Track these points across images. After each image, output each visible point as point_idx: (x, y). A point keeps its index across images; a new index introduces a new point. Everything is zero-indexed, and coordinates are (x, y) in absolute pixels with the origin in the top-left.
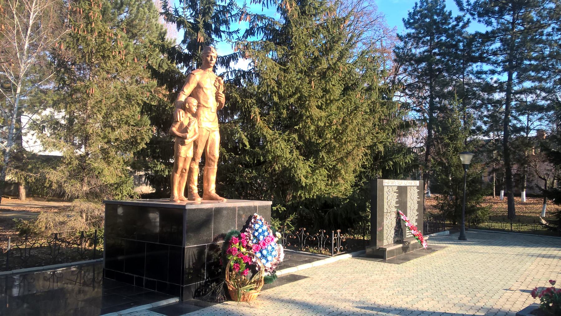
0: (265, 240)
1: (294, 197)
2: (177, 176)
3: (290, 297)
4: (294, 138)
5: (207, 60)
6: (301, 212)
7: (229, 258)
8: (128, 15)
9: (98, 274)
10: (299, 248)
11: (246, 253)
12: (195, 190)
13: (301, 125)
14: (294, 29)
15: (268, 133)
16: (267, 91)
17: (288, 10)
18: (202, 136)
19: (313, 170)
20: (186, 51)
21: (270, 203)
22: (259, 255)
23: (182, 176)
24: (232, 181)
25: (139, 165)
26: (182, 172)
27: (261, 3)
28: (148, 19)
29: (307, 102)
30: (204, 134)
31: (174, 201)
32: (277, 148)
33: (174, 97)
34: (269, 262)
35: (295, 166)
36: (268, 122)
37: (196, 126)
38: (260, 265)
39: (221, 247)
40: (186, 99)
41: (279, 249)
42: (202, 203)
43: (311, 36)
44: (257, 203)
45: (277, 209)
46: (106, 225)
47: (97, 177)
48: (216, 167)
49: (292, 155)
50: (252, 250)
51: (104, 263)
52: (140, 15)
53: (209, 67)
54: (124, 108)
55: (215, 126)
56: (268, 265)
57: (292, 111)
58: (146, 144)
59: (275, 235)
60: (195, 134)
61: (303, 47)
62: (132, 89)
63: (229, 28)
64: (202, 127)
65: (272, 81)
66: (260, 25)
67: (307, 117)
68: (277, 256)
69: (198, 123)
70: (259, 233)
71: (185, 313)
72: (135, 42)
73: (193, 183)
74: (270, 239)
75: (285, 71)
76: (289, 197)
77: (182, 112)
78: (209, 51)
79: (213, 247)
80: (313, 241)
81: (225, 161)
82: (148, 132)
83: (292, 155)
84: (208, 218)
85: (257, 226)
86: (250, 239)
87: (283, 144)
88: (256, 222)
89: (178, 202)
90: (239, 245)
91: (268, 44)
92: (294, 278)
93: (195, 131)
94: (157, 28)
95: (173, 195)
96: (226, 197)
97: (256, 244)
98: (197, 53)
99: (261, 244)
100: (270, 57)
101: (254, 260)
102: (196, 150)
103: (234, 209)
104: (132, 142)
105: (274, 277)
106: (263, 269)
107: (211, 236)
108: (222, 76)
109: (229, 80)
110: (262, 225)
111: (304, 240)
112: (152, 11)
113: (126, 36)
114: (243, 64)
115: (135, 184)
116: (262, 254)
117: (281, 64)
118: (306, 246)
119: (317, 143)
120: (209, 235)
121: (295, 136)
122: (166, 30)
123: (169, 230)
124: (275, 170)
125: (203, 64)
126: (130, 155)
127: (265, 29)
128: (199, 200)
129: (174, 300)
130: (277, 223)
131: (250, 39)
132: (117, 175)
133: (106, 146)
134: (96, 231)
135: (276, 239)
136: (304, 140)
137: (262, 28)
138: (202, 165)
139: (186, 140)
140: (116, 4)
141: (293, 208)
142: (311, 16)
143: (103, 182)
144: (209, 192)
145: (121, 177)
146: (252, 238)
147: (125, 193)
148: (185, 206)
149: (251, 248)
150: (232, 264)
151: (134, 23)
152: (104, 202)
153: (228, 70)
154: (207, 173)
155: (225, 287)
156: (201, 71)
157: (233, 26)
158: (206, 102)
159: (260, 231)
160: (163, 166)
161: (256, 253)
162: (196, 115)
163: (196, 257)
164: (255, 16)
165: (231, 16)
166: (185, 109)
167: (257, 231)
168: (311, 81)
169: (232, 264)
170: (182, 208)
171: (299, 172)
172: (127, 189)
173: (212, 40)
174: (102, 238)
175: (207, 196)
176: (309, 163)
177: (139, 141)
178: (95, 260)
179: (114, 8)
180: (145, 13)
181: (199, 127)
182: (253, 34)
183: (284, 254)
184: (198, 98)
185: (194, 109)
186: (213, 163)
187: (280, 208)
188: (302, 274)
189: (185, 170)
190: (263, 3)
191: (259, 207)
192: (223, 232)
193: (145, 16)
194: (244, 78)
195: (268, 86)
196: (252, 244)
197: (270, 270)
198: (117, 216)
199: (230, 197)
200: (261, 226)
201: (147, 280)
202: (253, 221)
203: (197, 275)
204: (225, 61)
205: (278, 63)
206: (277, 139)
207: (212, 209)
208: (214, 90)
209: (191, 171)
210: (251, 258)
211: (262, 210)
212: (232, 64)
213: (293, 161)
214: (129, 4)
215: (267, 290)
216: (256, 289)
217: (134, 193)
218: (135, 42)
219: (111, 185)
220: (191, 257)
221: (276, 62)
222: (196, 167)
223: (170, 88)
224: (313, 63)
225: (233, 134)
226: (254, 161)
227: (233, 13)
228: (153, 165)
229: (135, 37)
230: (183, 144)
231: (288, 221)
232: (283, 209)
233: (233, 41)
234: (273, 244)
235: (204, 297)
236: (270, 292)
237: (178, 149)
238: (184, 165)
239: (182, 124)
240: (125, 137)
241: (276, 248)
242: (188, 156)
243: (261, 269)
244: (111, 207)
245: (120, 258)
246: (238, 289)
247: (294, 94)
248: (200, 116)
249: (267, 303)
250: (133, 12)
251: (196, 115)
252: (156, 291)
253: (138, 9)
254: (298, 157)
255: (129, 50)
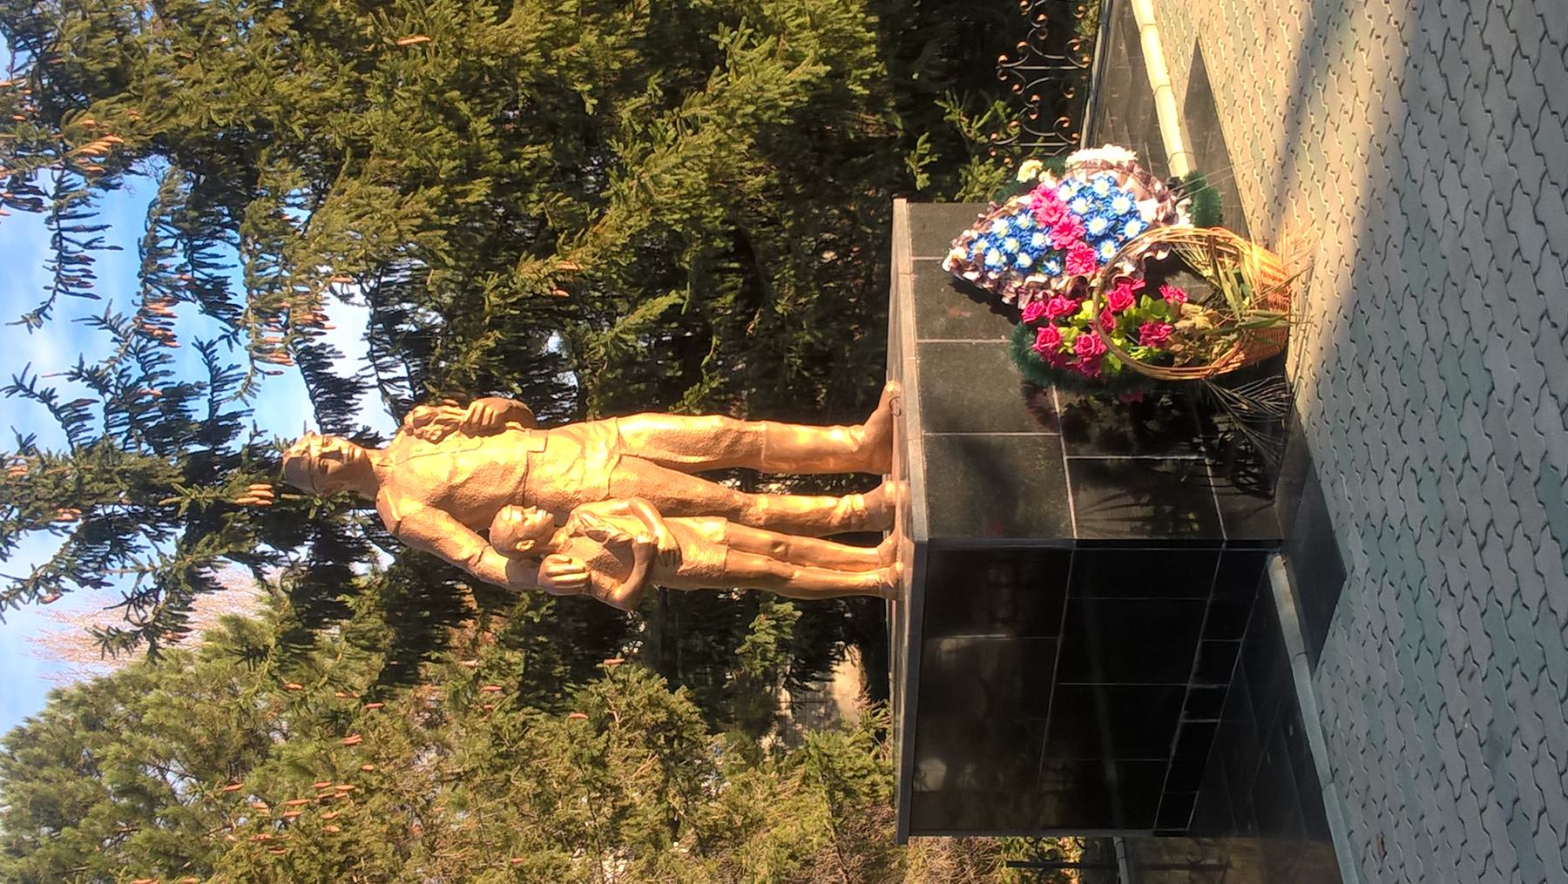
0: (1049, 225)
1: (874, 104)
2: (803, 575)
3: (1277, 120)
4: (634, 112)
5: (338, 473)
6: (934, 73)
7: (1118, 366)
8: (174, 765)
9: (1173, 851)
10: (1080, 80)
11: (1100, 300)
12: (855, 502)
13: (579, 87)
14: (186, 120)
15: (617, 224)
16: (449, 227)
17: (113, 145)
18: (641, 484)
19: (766, 27)
20: (303, 553)
21: (901, 206)
22: (1108, 250)
23: (799, 558)
24: (817, 358)
25: (752, 706)
26: (783, 558)
27: (88, 253)
28: (185, 688)
29: (487, 60)
30: (634, 477)
31: (899, 582)
32: (680, 183)
33: (492, 594)
34: (1139, 206)
35: (750, 109)
36: (577, 225)
37: (602, 508)
38: (1148, 241)
39: (1075, 400)
40: (501, 551)
41: (1086, 165)
42: (905, 476)
43: (210, 47)
44: (903, 259)
45: (925, 169)
46: (990, 828)
47: (808, 863)
48: (762, 427)
49: (706, 120)
50: (1089, 275)
51: (1131, 834)
52: (171, 723)
53: (365, 462)
54: (541, 776)
55: (602, 434)
56: (1149, 209)
57: (524, 118)
58: (672, 688)
59: (1031, 186)
60: (633, 511)
61: (255, 81)
62: (468, 744)
63: (200, 386)
64: (605, 483)
65: (406, 209)
66: (180, 259)
67: (549, 61)
68: (1114, 174)
69: (589, 501)
70: (1023, 247)
71: (1331, 532)
72: (277, 736)
73: (828, 513)
74: (1046, 204)
75: (362, 151)
76: (872, 125)
77: (550, 565)
78: (304, 466)
79: (1074, 426)
80: (1049, 23)
81: (734, 386)
82: (629, 683)
83: (706, 120)
84: (961, 445)
85: (994, 258)
86: (1047, 285)
87: (663, 160)
88: (979, 263)
89: (903, 567)
90: (1068, 325)
91: (255, 225)
92: (1201, 104)
93: (622, 513)
94: (218, 656)
95: (875, 588)
96: (882, 383)
97: (1063, 263)
98: (312, 512)
99: (1065, 240)
100: (304, 215)
101: (1128, 268)
102: (699, 505)
103: (925, 352)
104: (674, 748)
105: (1193, 185)
106: (1164, 233)
107: (1033, 441)
108: (399, 409)
109: (410, 378)
110: (993, 239)
111: (1046, 62)
112: (153, 677)
113: (258, 771)
114: (347, 328)
115: (828, 716)
116: (1105, 237)
117: (333, 172)
118: (1072, 53)
119: (652, 15)
120: (1029, 444)
121: (625, 112)
122: (226, 620)
123: (1005, 593)
124: (767, 188)
125: (360, 483)
126: (719, 747)
127: (196, 234)
128: (890, 488)
129: (1280, 576)
130: (981, 173)
131: (238, 294)
132: (799, 792)
133: (690, 836)
134: (1009, 864)
135: (1048, 181)
136: (639, 69)
137: (191, 250)
138: (752, 480)
139: (661, 546)
140: (135, 811)
141: (920, 109)
142: (127, 47)
143: (826, 841)
144: (862, 448)
145: (805, 778)
146: (1040, 278)
147: (867, 759)
148: (919, 546)
149: (1082, 281)
150: (1140, 352)
151: (204, 741)
152: (902, 839)
153: (373, 381)
154: (785, 459)
155: (1231, 380)
156: (385, 493)
157: (188, 368)
158: (508, 470)
159: (1011, 245)
160: (762, 622)
161: (1099, 262)
162: (561, 510)
163: (1113, 491)
164: (146, 281)
165: (148, 378)
166: (534, 558)
167: (1012, 258)
168: (399, 48)
169: (1140, 352)
170: (925, 554)
171: (773, 92)
172: (848, 750)
173: (252, 449)
174: (1038, 841)
175: (877, 459)
176: (736, 49)
177: (662, 716)
178: (1122, 864)
179: (151, 818)
180: (162, 704)
181: (608, 498)
182: (220, 285)
183: (1108, 147)
184: (494, 505)
185: (537, 518)
186: (747, 439)
187: (922, 158)
188: (1185, 66)
189: (776, 544)
190: (88, 245)
191: (917, 250)
192: (1016, 392)
193: (175, 701)
194: (401, 316)
195: (427, 225)
196: (1066, 278)
197: (1168, 204)
198: (949, 789)
199: (875, 364)
200: (994, 240)
201: (1201, 676)
202: (971, 276)
203: (1187, 488)
204: (334, 397)
205: (332, 182)
206: (643, 187)
207: (927, 442)
208: (454, 441)
209: (779, 523)
210: (1120, 280)
211: (930, 241)
212: (342, 369)
213: (731, 115)
214: (132, 762)
215: (1248, 213)
216: (1237, 258)
217: (867, 728)
218: (277, 736)
219: (837, 813)
220: (1117, 513)
221: (327, 191)
222: (764, 503)
223: (459, 614)
224: (320, 36)
225: (629, 360)
226: (732, 270)
227: (136, 372)
228: (757, 662)
229: (260, 739)
230: (674, 556)
231: (971, 129)
232: (923, 146)
233: (246, 368)
234: (1064, 194)
235: (1270, 460)
236: (1253, 202)
237: (698, 575)
238: (758, 550)
239: (597, 564)
240: (649, 766)
241: (1081, 177)
242: (720, 538)
243: (1164, 239)
244: (921, 813)
245: (1112, 773)
246: (1239, 330)
247: (450, 113)
248: (563, 494)
249: (1297, 212)
250: (160, 748)
251: (561, 510)
252: (1242, 641)
253: (147, 729)
254: (715, 98)
255: (313, 757)
